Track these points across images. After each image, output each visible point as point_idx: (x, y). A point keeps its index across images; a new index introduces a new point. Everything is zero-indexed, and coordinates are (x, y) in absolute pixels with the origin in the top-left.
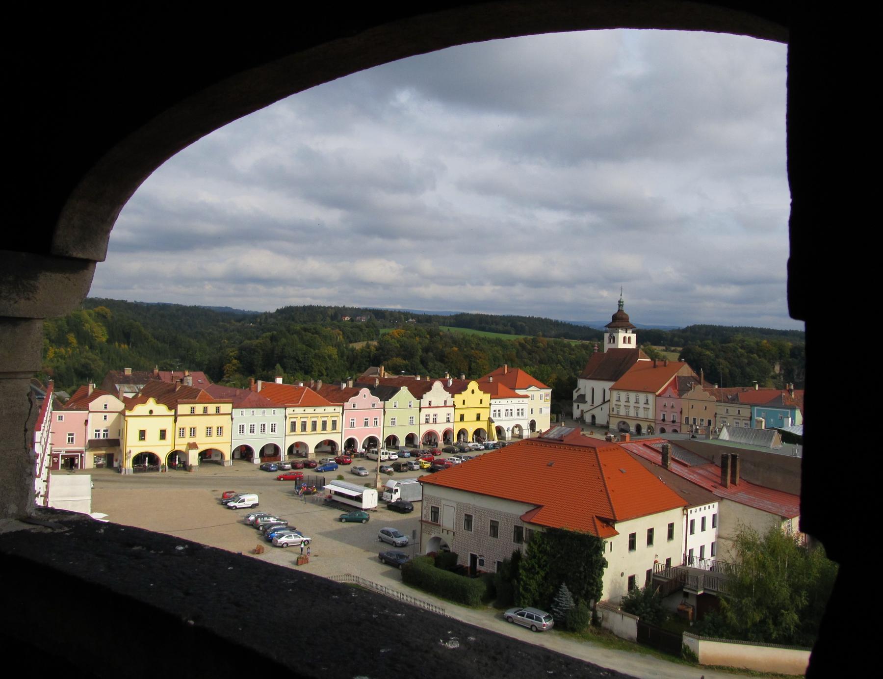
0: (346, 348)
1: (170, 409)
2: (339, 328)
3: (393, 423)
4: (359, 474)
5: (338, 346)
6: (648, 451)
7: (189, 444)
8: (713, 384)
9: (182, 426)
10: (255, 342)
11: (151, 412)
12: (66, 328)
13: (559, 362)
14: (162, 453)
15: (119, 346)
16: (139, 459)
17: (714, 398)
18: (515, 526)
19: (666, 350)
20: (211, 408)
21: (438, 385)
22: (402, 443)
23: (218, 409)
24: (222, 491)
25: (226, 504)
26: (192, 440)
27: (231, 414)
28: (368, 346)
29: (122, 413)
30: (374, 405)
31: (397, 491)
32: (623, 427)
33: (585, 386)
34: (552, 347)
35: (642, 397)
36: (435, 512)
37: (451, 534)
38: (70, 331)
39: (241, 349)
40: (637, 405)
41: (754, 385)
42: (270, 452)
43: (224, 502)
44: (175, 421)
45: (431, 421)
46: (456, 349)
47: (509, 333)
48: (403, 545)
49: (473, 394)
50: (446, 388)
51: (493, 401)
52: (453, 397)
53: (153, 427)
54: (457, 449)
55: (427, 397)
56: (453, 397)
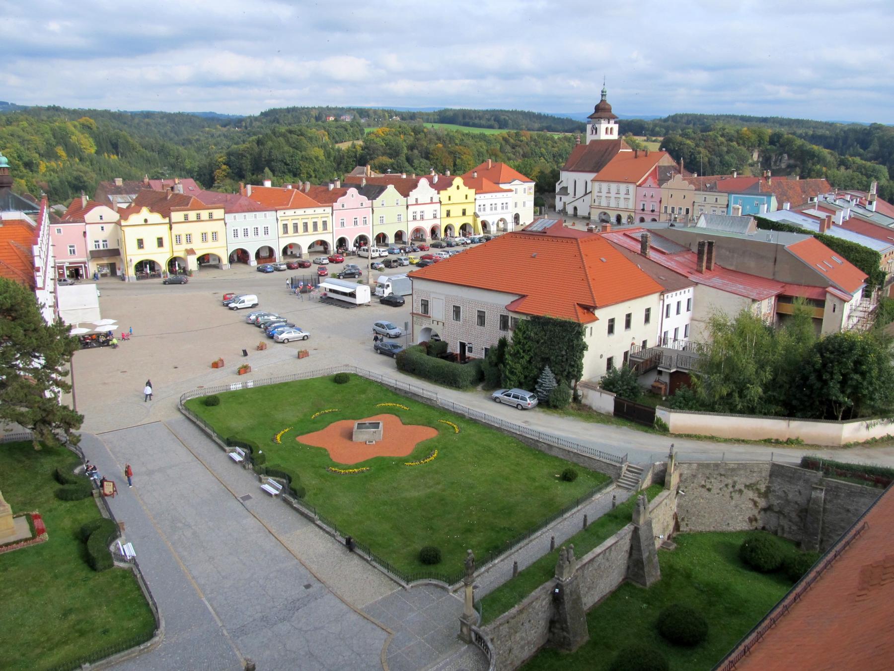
3: (382, 221)
5: (324, 146)
6: (628, 240)
9: (178, 233)
10: (242, 147)
11: (146, 221)
12: (53, 141)
14: (162, 259)
16: (140, 266)
17: (692, 187)
19: (647, 140)
20: (204, 214)
21: (423, 182)
22: (391, 240)
23: (211, 215)
25: (227, 305)
26: (189, 247)
27: (224, 219)
28: (354, 146)
29: (118, 223)
30: (362, 204)
31: (388, 286)
32: (604, 217)
34: (535, 140)
35: (623, 187)
36: (425, 305)
38: (58, 143)
39: (229, 154)
40: (618, 196)
41: (732, 173)
42: (265, 254)
43: (226, 303)
44: (171, 228)
45: (418, 217)
46: (440, 145)
47: (491, 127)
48: (397, 336)
49: (459, 190)
50: (432, 185)
51: (478, 196)
52: (438, 193)
53: (150, 235)
54: (444, 244)
55: (414, 194)
56: (438, 193)
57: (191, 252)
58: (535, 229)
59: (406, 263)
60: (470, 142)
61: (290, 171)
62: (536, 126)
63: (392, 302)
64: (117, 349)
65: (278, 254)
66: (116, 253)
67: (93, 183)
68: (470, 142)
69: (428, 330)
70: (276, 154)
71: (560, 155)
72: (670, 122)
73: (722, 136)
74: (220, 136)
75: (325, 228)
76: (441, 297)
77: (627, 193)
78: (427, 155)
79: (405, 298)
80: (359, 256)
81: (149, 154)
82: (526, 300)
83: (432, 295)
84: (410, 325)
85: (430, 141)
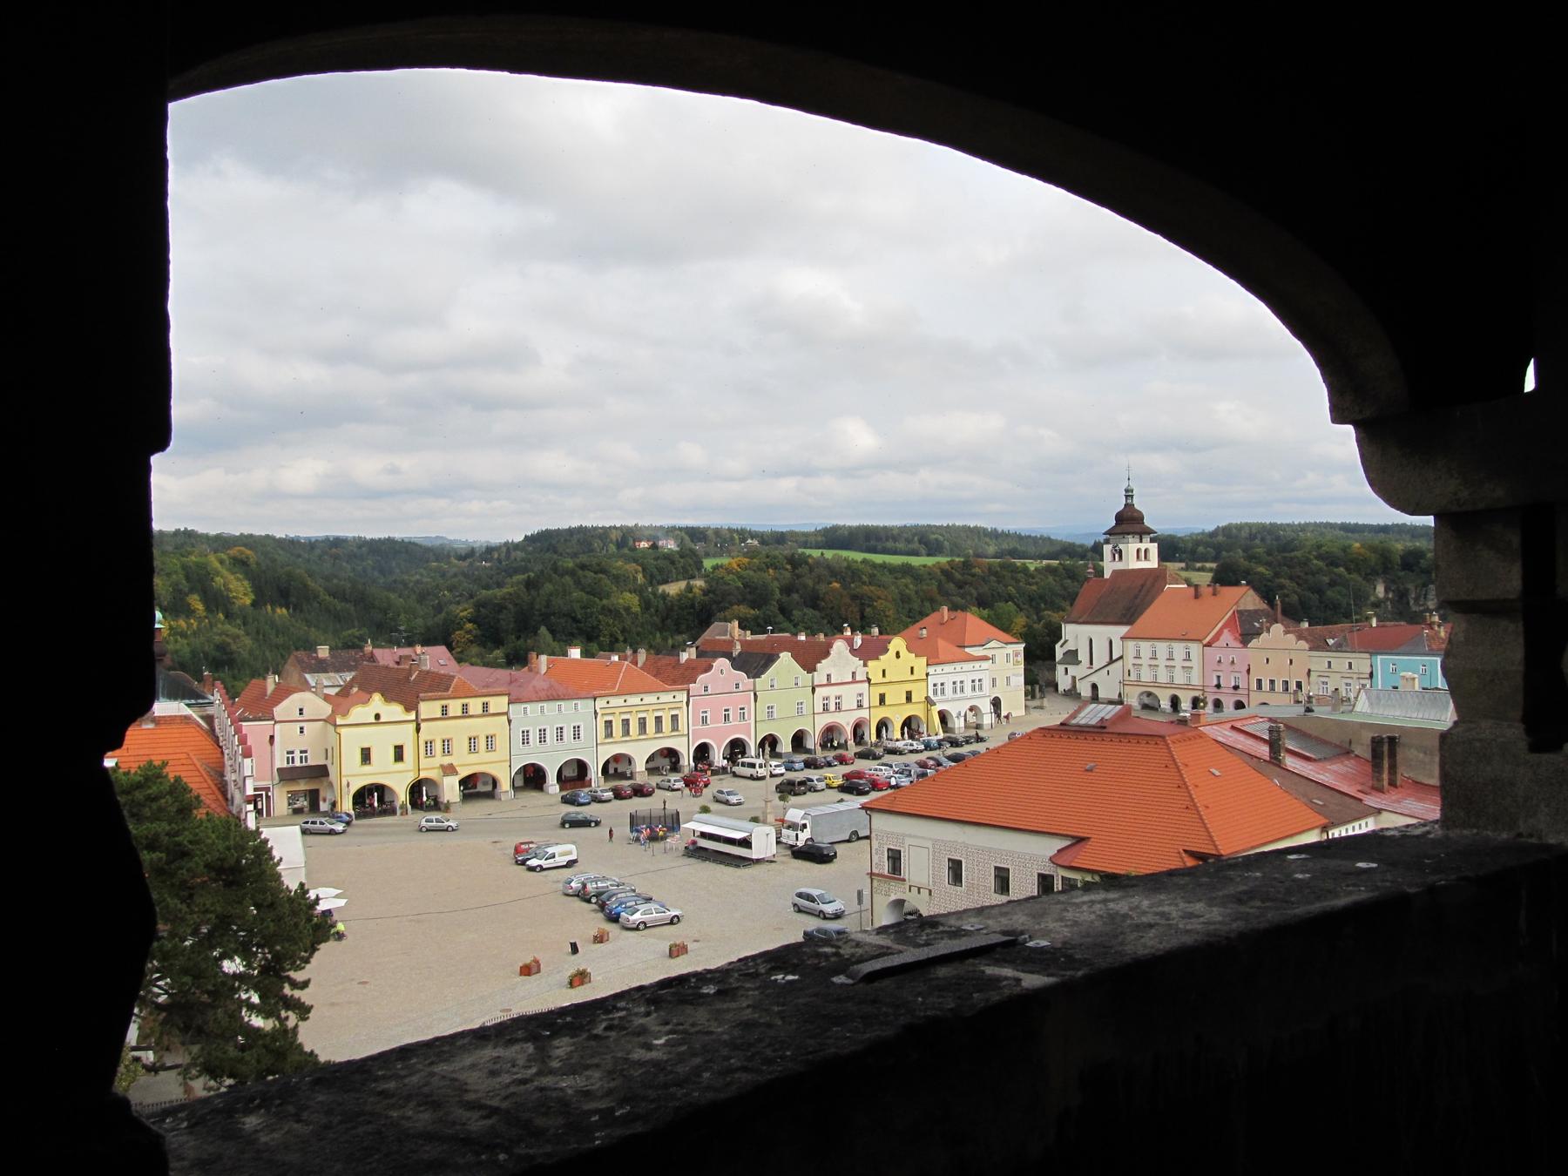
0: (654, 594)
1: (408, 710)
2: (635, 561)
3: (770, 714)
4: (727, 803)
5: (639, 591)
6: (1241, 738)
7: (442, 766)
8: (1299, 621)
9: (429, 738)
10: (499, 593)
11: (377, 716)
12: (184, 585)
13: (1010, 598)
14: (400, 784)
15: (274, 611)
16: (361, 797)
17: (1303, 644)
18: (1040, 875)
19: (1186, 569)
20: (475, 705)
21: (839, 646)
22: (785, 746)
23: (485, 706)
24: (511, 842)
25: (523, 863)
26: (447, 760)
28: (689, 589)
29: (330, 720)
30: (737, 686)
31: (805, 826)
32: (1146, 700)
33: (1074, 635)
34: (996, 574)
35: (1179, 648)
36: (895, 858)
37: (925, 893)
38: (192, 591)
39: (480, 605)
40: (1154, 662)
41: (1368, 618)
42: (570, 773)
43: (521, 857)
44: (418, 730)
45: (832, 707)
46: (836, 585)
47: (916, 553)
48: (837, 916)
49: (899, 658)
50: (853, 652)
51: (931, 670)
52: (865, 665)
53: (380, 742)
54: (879, 751)
55: (824, 667)
56: (865, 665)
57: (449, 770)
58: (1083, 722)
59: (821, 785)
60: (887, 579)
61: (581, 632)
62: (991, 549)
63: (813, 854)
64: (344, 942)
65: (595, 773)
66: (321, 772)
67: (245, 655)
68: (887, 579)
69: (899, 903)
70: (558, 602)
71: (1042, 597)
72: (1220, 538)
73: (1319, 557)
74: (455, 575)
75: (675, 728)
76: (924, 845)
77: (1188, 659)
78: (814, 601)
79: (838, 848)
80: (735, 775)
81: (339, 605)
82: (1088, 846)
83: (908, 841)
84: (866, 893)
85: (819, 579)
